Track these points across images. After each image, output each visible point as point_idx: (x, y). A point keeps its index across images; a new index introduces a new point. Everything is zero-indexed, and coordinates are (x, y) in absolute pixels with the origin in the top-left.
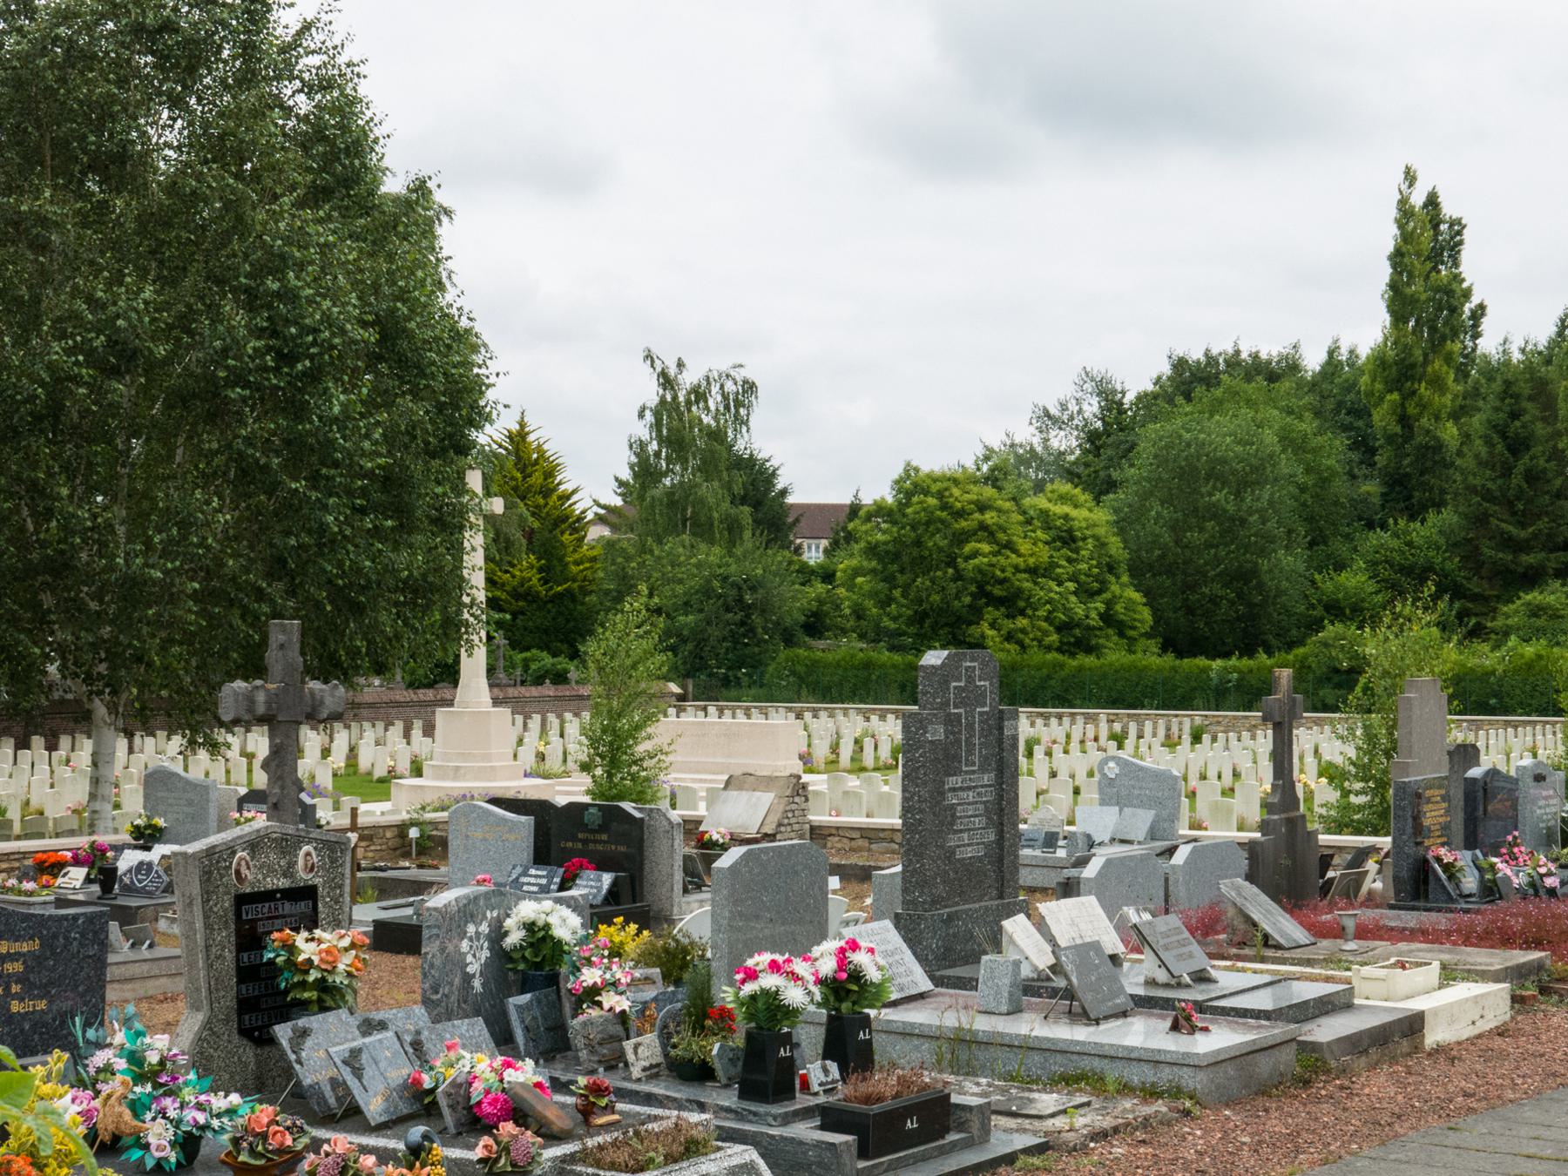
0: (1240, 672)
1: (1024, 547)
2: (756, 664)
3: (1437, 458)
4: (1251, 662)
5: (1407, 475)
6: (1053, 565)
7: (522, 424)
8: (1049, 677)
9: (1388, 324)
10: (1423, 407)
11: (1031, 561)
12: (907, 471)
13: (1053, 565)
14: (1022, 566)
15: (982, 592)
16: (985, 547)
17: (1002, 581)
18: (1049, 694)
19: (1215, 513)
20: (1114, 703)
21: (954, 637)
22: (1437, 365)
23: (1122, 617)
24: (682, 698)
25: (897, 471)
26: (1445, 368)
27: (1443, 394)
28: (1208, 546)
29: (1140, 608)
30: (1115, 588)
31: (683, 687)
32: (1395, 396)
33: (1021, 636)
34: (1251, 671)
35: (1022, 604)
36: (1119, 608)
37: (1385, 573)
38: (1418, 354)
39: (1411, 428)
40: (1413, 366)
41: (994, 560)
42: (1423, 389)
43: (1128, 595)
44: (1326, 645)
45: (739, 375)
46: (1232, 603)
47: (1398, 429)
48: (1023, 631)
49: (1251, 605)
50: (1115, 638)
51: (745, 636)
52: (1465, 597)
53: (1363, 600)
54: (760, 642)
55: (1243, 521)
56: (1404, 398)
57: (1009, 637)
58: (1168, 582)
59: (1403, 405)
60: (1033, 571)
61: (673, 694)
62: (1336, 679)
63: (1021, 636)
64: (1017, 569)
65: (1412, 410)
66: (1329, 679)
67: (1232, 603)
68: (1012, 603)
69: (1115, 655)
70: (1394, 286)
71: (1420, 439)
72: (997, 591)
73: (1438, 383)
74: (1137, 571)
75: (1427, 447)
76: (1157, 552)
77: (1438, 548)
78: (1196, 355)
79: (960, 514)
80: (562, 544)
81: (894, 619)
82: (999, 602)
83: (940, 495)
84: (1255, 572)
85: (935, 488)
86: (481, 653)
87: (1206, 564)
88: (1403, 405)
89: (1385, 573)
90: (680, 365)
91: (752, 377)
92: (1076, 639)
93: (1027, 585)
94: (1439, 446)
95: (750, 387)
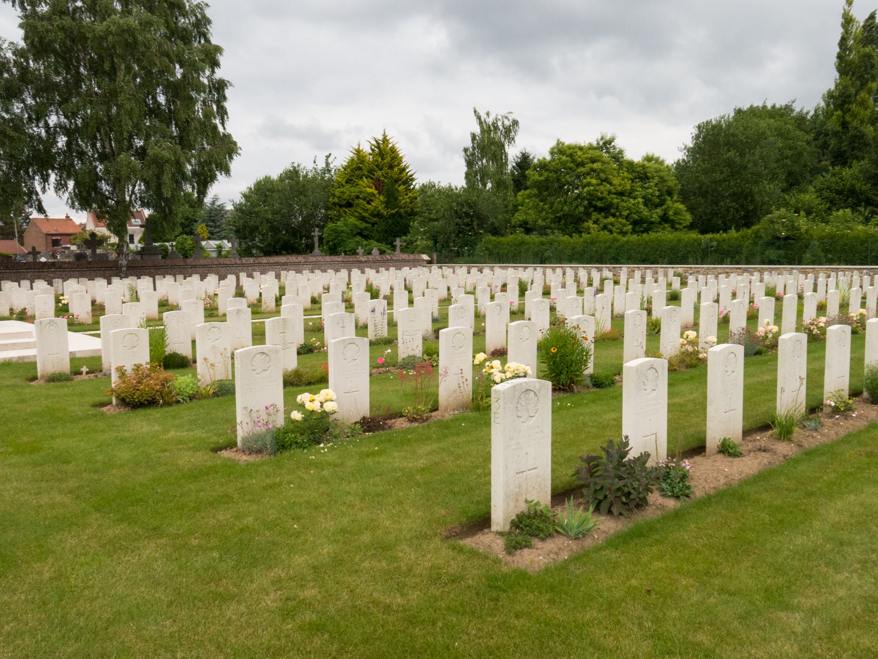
0: (717, 241)
1: (616, 181)
2: (472, 245)
3: (861, 141)
4: (725, 235)
5: (845, 151)
6: (633, 190)
7: (385, 136)
8: (610, 247)
9: (838, 77)
10: (854, 116)
11: (619, 188)
12: (558, 144)
13: (633, 190)
14: (614, 191)
15: (590, 204)
16: (594, 181)
17: (601, 199)
18: (609, 256)
19: (729, 163)
20: (644, 261)
21: (576, 229)
22: (862, 95)
23: (672, 217)
24: (430, 262)
25: (553, 143)
26: (867, 96)
27: (866, 109)
28: (725, 180)
29: (685, 213)
30: (669, 202)
31: (431, 256)
32: (839, 112)
33: (610, 226)
34: (724, 240)
35: (612, 211)
36: (671, 213)
37: (826, 194)
38: (853, 91)
39: (847, 128)
40: (849, 96)
41: (598, 188)
42: (853, 107)
43: (676, 206)
44: (772, 222)
45: (511, 117)
46: (737, 210)
47: (840, 129)
48: (612, 224)
49: (748, 212)
50: (669, 229)
51: (470, 231)
52: (873, 205)
53: (812, 208)
54: (476, 234)
55: (745, 168)
56: (844, 113)
57: (605, 227)
58: (703, 201)
59: (843, 117)
60: (621, 194)
61: (424, 260)
62: (777, 244)
63: (610, 226)
64: (610, 193)
65: (848, 118)
66: (773, 244)
67: (737, 210)
68: (607, 210)
69: (666, 235)
70: (840, 57)
71: (852, 132)
72: (599, 204)
73: (863, 104)
74: (685, 197)
75: (856, 136)
76: (697, 185)
77: (858, 180)
78: (745, 107)
79: (582, 164)
80: (398, 190)
81: (544, 220)
82: (600, 210)
83: (571, 155)
84: (751, 194)
85: (569, 152)
86: (91, 227)
87: (723, 190)
88: (843, 117)
89: (826, 194)
90: (488, 114)
91: (517, 118)
92: (640, 225)
93: (615, 201)
94: (863, 135)
95: (515, 123)
